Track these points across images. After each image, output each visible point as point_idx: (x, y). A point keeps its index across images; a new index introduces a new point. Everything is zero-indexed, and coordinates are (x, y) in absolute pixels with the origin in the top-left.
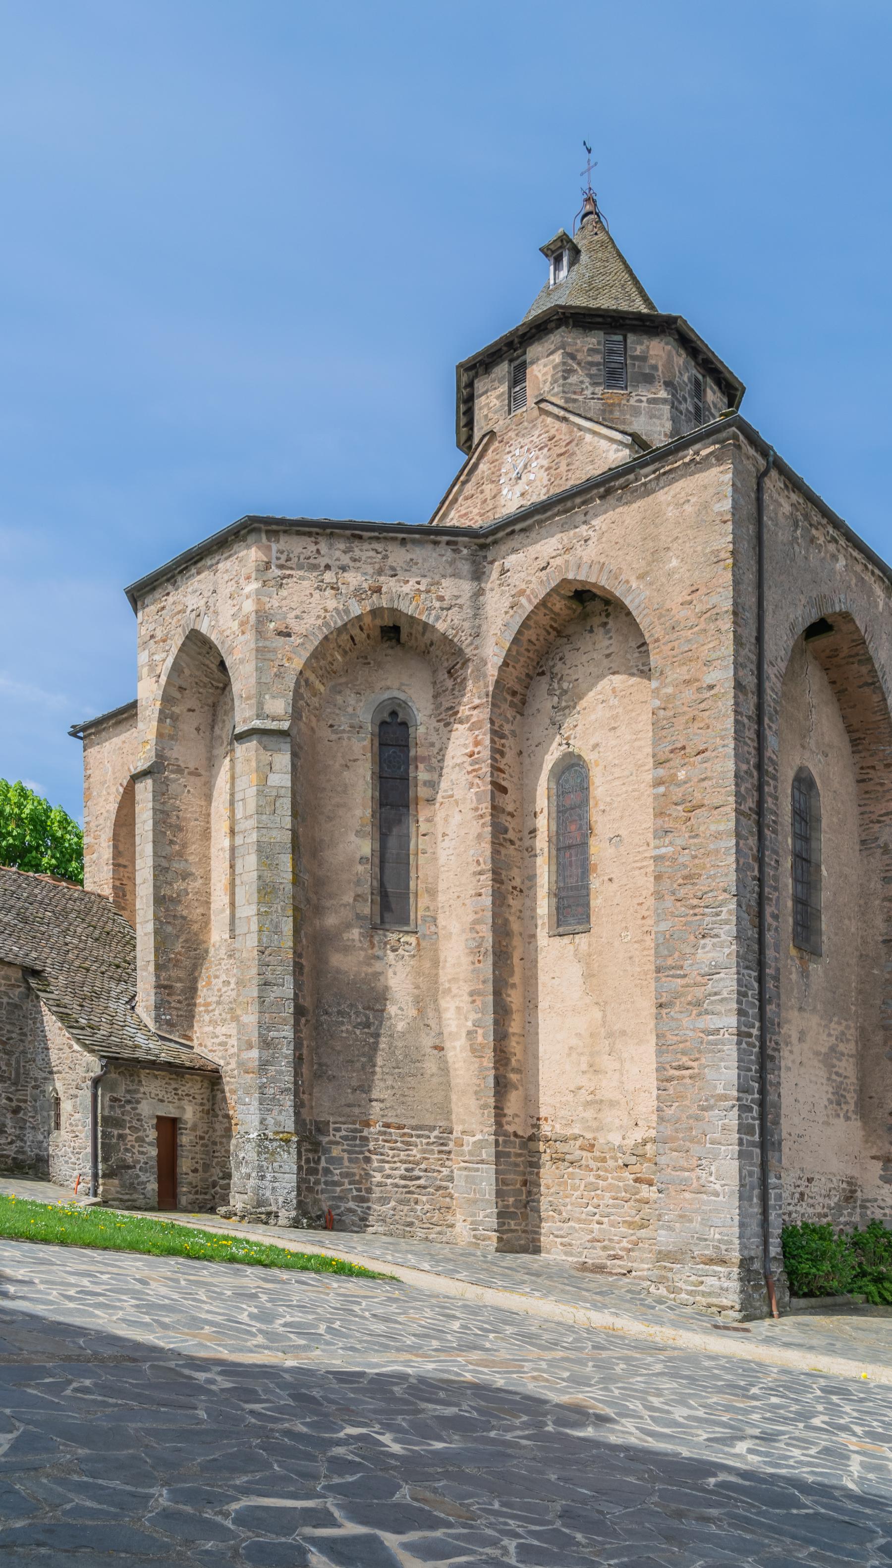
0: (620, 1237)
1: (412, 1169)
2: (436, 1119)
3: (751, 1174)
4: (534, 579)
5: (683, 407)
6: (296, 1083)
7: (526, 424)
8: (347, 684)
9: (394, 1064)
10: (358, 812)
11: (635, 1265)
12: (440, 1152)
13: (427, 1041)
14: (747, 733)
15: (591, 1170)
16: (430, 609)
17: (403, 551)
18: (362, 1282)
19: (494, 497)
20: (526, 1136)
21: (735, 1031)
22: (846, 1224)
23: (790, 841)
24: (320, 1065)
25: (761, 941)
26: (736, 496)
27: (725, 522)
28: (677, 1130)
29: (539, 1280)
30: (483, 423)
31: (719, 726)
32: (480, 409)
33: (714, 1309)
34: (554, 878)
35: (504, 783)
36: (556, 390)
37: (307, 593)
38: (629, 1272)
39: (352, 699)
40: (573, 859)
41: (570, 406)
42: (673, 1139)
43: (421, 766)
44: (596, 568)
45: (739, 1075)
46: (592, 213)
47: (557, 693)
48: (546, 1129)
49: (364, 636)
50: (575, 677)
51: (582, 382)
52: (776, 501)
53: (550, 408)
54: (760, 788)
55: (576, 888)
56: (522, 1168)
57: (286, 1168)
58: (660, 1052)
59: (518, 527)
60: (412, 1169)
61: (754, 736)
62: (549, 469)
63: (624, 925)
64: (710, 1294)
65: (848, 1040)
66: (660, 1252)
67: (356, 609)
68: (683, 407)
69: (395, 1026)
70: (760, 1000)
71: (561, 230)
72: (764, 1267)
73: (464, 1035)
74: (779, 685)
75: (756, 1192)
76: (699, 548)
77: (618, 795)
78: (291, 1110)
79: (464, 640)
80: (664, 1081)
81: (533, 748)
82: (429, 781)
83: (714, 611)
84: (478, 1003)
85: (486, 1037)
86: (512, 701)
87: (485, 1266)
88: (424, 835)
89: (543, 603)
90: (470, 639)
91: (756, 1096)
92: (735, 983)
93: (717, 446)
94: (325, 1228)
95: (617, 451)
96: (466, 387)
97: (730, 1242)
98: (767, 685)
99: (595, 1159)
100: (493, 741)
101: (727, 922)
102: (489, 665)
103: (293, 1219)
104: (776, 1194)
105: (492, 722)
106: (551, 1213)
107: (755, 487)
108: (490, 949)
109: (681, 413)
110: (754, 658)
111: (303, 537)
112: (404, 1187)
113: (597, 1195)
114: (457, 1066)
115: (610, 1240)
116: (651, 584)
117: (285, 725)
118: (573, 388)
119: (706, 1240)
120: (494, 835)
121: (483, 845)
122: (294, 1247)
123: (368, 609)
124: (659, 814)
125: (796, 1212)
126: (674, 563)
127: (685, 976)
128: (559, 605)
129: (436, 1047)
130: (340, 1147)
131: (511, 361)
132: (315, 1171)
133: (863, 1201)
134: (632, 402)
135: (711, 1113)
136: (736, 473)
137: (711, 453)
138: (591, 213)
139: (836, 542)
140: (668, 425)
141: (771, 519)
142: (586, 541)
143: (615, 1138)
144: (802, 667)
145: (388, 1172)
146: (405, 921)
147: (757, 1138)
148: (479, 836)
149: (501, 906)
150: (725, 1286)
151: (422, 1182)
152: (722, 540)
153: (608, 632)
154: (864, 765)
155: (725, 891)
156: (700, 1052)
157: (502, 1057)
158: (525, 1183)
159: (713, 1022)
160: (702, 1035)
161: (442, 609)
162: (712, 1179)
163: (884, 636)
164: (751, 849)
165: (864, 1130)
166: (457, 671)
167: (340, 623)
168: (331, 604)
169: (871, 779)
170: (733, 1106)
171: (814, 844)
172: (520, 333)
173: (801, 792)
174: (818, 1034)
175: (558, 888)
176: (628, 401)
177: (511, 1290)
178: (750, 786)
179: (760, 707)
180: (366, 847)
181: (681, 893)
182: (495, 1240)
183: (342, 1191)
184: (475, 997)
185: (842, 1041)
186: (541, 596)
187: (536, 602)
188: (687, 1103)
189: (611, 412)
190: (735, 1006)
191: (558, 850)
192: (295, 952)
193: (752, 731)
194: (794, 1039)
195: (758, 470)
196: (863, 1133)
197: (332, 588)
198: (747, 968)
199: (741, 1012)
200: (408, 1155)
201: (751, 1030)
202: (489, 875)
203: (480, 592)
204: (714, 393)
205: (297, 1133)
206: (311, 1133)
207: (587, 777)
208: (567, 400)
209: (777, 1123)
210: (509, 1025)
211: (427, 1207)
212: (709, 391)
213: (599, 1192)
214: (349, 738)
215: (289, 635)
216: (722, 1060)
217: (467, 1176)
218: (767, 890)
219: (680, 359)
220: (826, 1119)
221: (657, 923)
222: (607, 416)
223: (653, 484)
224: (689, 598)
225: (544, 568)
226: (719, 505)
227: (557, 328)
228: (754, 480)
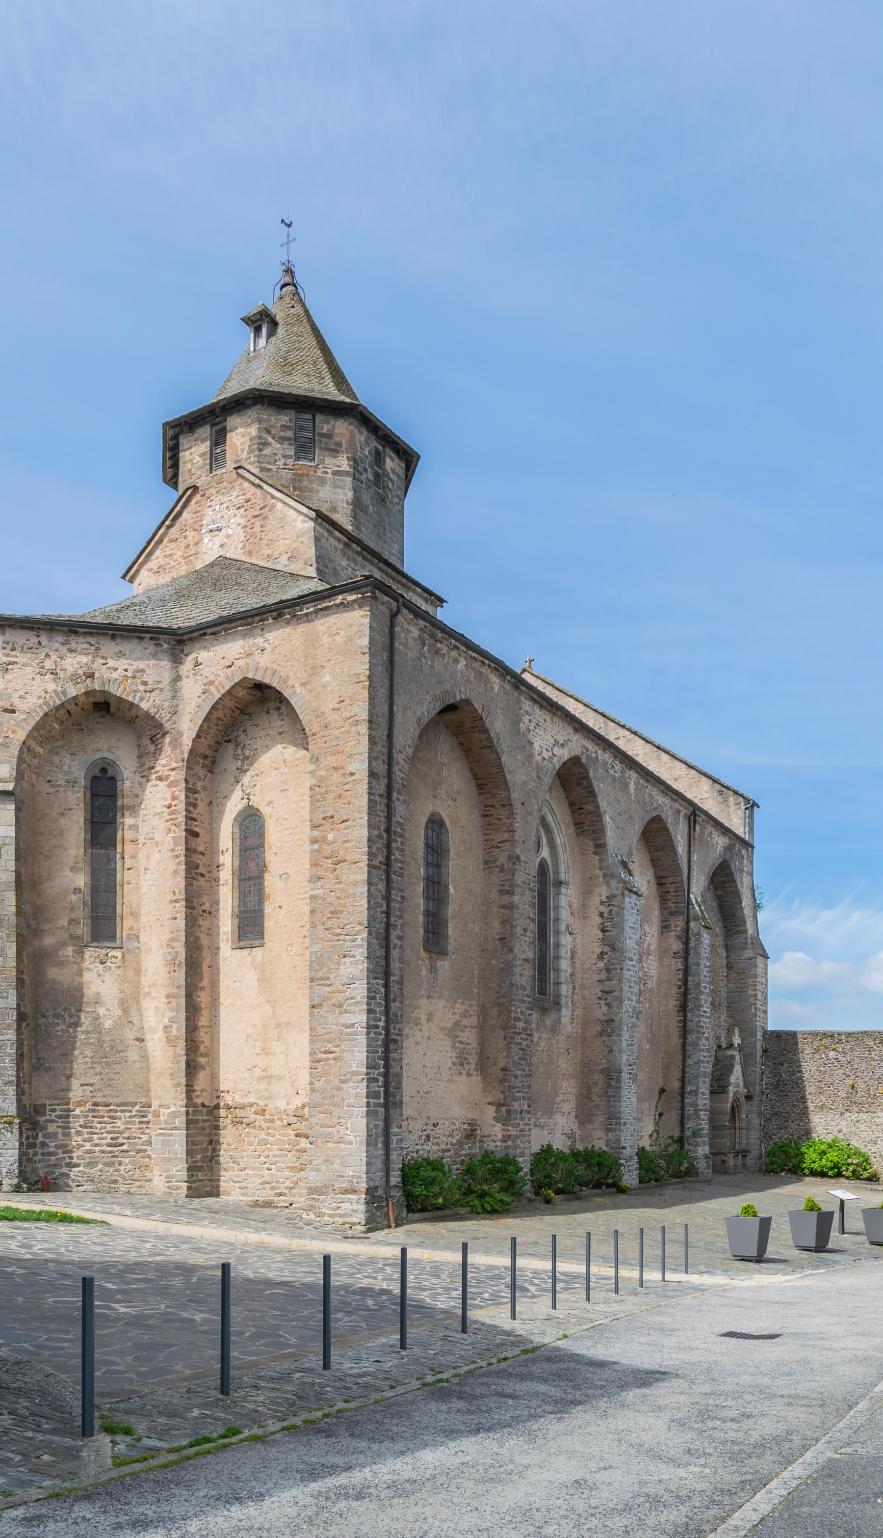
0: (284, 1178)
1: (117, 1138)
2: (137, 1097)
3: (376, 1127)
4: (221, 674)
5: (363, 477)
6: (18, 1076)
7: (225, 484)
8: (63, 746)
9: (102, 1055)
10: (72, 852)
11: (295, 1199)
12: (140, 1123)
13: (130, 1035)
14: (379, 807)
15: (263, 1129)
16: (135, 691)
17: (113, 644)
18: (80, 1226)
19: (197, 544)
20: (212, 1105)
21: (365, 1025)
22: (467, 1155)
23: (422, 870)
24: (38, 1059)
25: (387, 958)
26: (373, 634)
27: (364, 654)
28: (324, 1098)
29: (217, 1216)
30: (187, 477)
31: (358, 804)
32: (184, 463)
33: (347, 1226)
34: (236, 903)
35: (196, 829)
36: (252, 459)
37: (30, 677)
38: (291, 1205)
39: (67, 759)
40: (252, 888)
41: (260, 475)
42: (321, 1105)
43: (127, 813)
44: (270, 672)
45: (368, 1057)
46: (290, 281)
47: (241, 758)
48: (228, 1099)
49: (79, 709)
50: (255, 747)
51: (275, 454)
52: (407, 630)
53: (247, 475)
54: (388, 846)
55: (254, 912)
56: (208, 1131)
57: (10, 1145)
58: (312, 1041)
59: (209, 631)
60: (117, 1138)
61: (385, 809)
62: (245, 527)
63: (290, 942)
64: (344, 1215)
65: (470, 1016)
66: (310, 1188)
67: (73, 691)
68: (363, 477)
69: (103, 1024)
70: (386, 1001)
71: (261, 303)
72: (386, 1193)
73: (161, 1029)
74: (406, 766)
75: (381, 1139)
76: (345, 670)
77: (287, 842)
78: (14, 1098)
79: (163, 717)
80: (315, 1061)
81: (221, 799)
82: (134, 826)
83: (355, 719)
84: (173, 1004)
85: (179, 1030)
86: (203, 763)
87: (175, 1209)
88: (129, 869)
89: (229, 692)
90: (169, 716)
91: (382, 1070)
92: (365, 991)
93: (359, 596)
94: (42, 1191)
95: (303, 522)
96: (172, 439)
97: (360, 1177)
98: (396, 768)
99: (266, 1121)
100: (187, 797)
101: (360, 946)
102: (185, 737)
103: (16, 1185)
104: (397, 1139)
105: (187, 782)
106: (232, 1164)
107: (389, 624)
108: (183, 962)
109: (362, 482)
110: (385, 750)
111: (26, 631)
112: (110, 1152)
113: (267, 1149)
114: (155, 1053)
115: (276, 1182)
116: (310, 691)
117: (10, 787)
118: (267, 459)
119: (343, 1176)
120: (187, 871)
121: (178, 879)
122: (23, 1207)
123: (83, 691)
124: (314, 864)
125: (423, 1150)
126: (328, 678)
127: (331, 985)
128: (241, 693)
129: (137, 1039)
130: (55, 1125)
131: (213, 425)
132: (33, 1146)
133: (482, 1137)
134: (319, 473)
135: (348, 1085)
136: (373, 617)
137: (355, 601)
138: (289, 284)
139: (458, 648)
140: (350, 495)
141: (402, 644)
142: (262, 650)
143: (281, 1105)
144: (436, 736)
145: (97, 1141)
146: (113, 938)
147: (382, 1100)
148: (175, 872)
149: (192, 927)
150: (356, 1208)
151: (125, 1147)
152: (362, 666)
153: (280, 715)
154: (487, 804)
155: (359, 924)
156: (340, 1040)
157: (192, 1045)
158: (211, 1142)
159: (349, 1019)
160: (342, 1028)
161: (146, 692)
162: (348, 1132)
163: (499, 711)
164: (381, 892)
165: (483, 1082)
166: (158, 739)
167: (58, 703)
168: (51, 687)
169: (492, 815)
170: (363, 1079)
171: (443, 870)
172: (220, 405)
173: (433, 830)
174: (444, 1013)
175: (240, 911)
176: (315, 472)
177: (193, 1224)
178: (380, 846)
179: (389, 787)
180: (81, 880)
181: (329, 924)
182: (186, 1189)
183: (57, 1159)
184: (170, 999)
185: (465, 1017)
186: (227, 688)
187: (223, 692)
188: (331, 1078)
189: (301, 481)
190: (366, 1007)
191: (240, 880)
192: (17, 971)
193: (383, 805)
194: (423, 1020)
195: (391, 611)
196: (482, 1085)
197: (52, 673)
198: (376, 978)
199: (369, 1011)
200: (114, 1127)
201: (379, 1023)
202: (183, 903)
203: (177, 679)
204: (393, 460)
205: (19, 1116)
206: (30, 1115)
207: (263, 825)
208: (262, 470)
209: (399, 1087)
210: (199, 1020)
211: (129, 1167)
212: (388, 460)
213: (269, 1146)
214: (65, 791)
215: (13, 712)
216: (356, 1046)
217: (163, 1141)
218: (392, 919)
219: (362, 436)
220: (450, 1077)
221: (312, 945)
222: (297, 484)
223: (313, 616)
224: (338, 706)
225: (229, 666)
226: (359, 640)
227: (255, 404)
228: (388, 619)
